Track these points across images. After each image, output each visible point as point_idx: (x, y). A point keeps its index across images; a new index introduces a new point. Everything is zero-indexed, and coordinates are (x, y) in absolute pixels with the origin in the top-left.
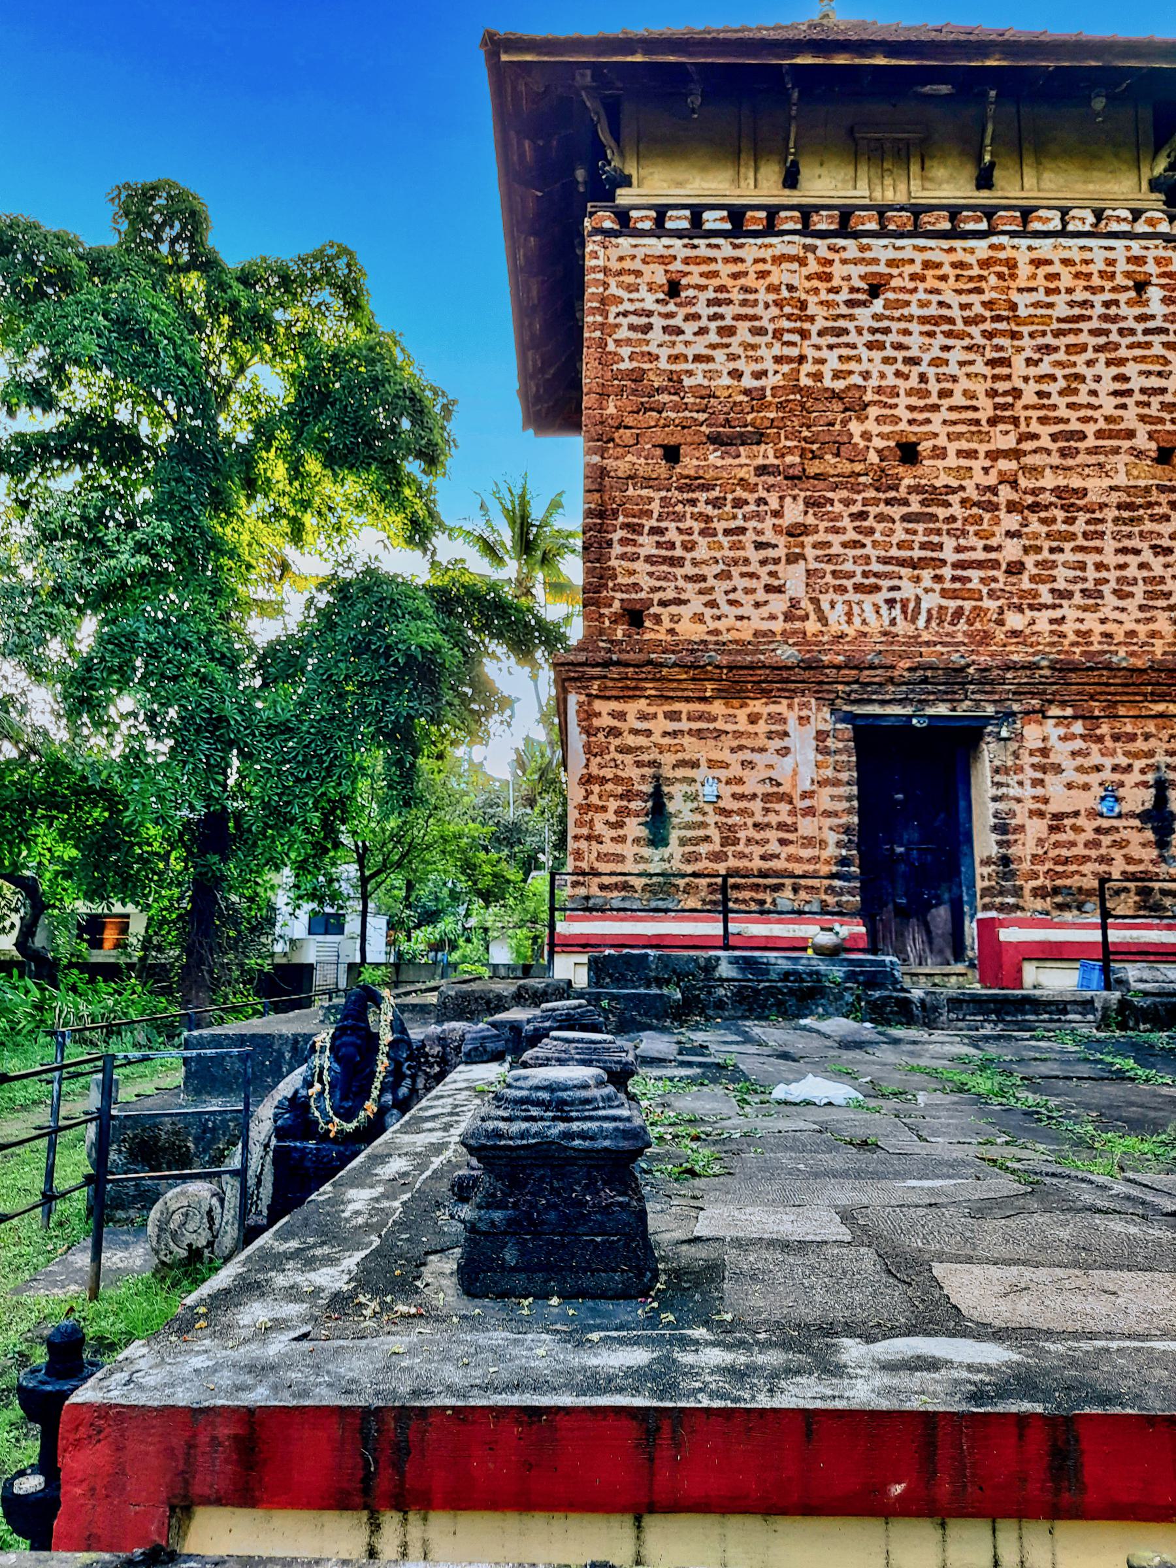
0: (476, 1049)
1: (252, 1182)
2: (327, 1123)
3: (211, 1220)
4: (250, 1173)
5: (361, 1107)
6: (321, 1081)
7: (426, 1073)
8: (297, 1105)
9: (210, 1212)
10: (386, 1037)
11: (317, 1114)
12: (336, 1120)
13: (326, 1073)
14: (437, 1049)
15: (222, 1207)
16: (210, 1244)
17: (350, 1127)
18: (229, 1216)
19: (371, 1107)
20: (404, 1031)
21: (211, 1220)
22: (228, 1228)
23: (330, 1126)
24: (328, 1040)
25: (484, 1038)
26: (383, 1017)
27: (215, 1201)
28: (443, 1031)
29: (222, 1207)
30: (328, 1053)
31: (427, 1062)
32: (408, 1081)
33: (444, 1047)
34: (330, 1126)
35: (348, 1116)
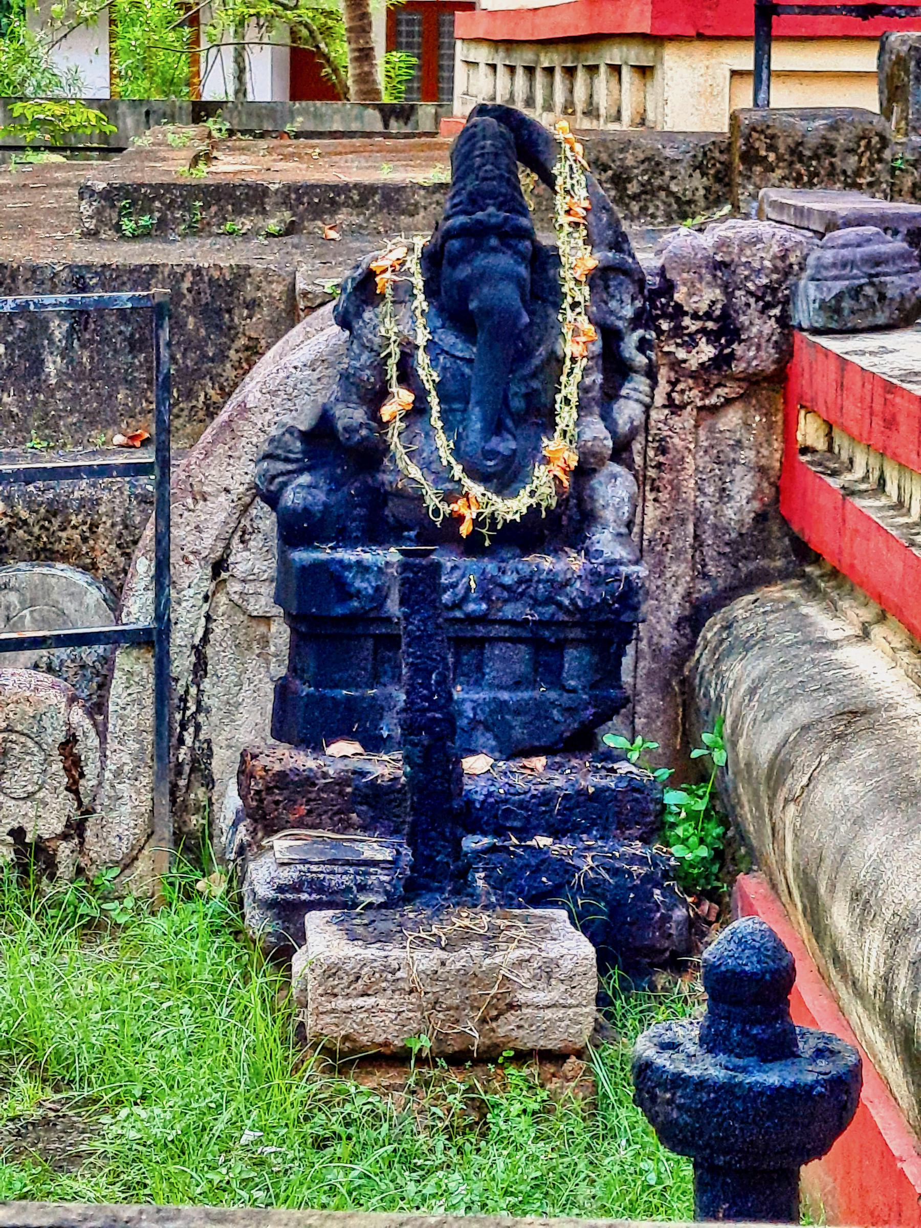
0: (856, 292)
1: (181, 664)
2: (448, 497)
3: (74, 765)
4: (179, 638)
5: (531, 454)
6: (407, 376)
7: (676, 365)
8: (338, 449)
9: (71, 740)
10: (578, 259)
11: (415, 472)
12: (476, 489)
13: (422, 358)
14: (707, 296)
15: (102, 734)
16: (75, 829)
17: (512, 508)
18: (122, 756)
19: (559, 451)
20: (619, 243)
21: (74, 765)
22: (124, 788)
23: (459, 506)
24: (413, 264)
25: (877, 261)
26: (561, 202)
27: (78, 716)
28: (722, 244)
29: (102, 734)
30: (421, 302)
31: (678, 331)
32: (640, 383)
33: (728, 290)
34: (459, 506)
35: (505, 476)
